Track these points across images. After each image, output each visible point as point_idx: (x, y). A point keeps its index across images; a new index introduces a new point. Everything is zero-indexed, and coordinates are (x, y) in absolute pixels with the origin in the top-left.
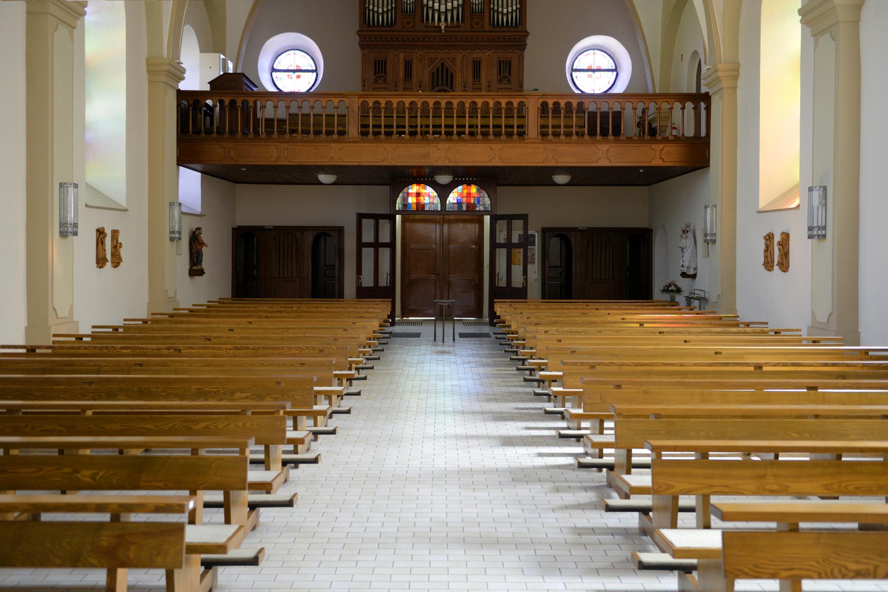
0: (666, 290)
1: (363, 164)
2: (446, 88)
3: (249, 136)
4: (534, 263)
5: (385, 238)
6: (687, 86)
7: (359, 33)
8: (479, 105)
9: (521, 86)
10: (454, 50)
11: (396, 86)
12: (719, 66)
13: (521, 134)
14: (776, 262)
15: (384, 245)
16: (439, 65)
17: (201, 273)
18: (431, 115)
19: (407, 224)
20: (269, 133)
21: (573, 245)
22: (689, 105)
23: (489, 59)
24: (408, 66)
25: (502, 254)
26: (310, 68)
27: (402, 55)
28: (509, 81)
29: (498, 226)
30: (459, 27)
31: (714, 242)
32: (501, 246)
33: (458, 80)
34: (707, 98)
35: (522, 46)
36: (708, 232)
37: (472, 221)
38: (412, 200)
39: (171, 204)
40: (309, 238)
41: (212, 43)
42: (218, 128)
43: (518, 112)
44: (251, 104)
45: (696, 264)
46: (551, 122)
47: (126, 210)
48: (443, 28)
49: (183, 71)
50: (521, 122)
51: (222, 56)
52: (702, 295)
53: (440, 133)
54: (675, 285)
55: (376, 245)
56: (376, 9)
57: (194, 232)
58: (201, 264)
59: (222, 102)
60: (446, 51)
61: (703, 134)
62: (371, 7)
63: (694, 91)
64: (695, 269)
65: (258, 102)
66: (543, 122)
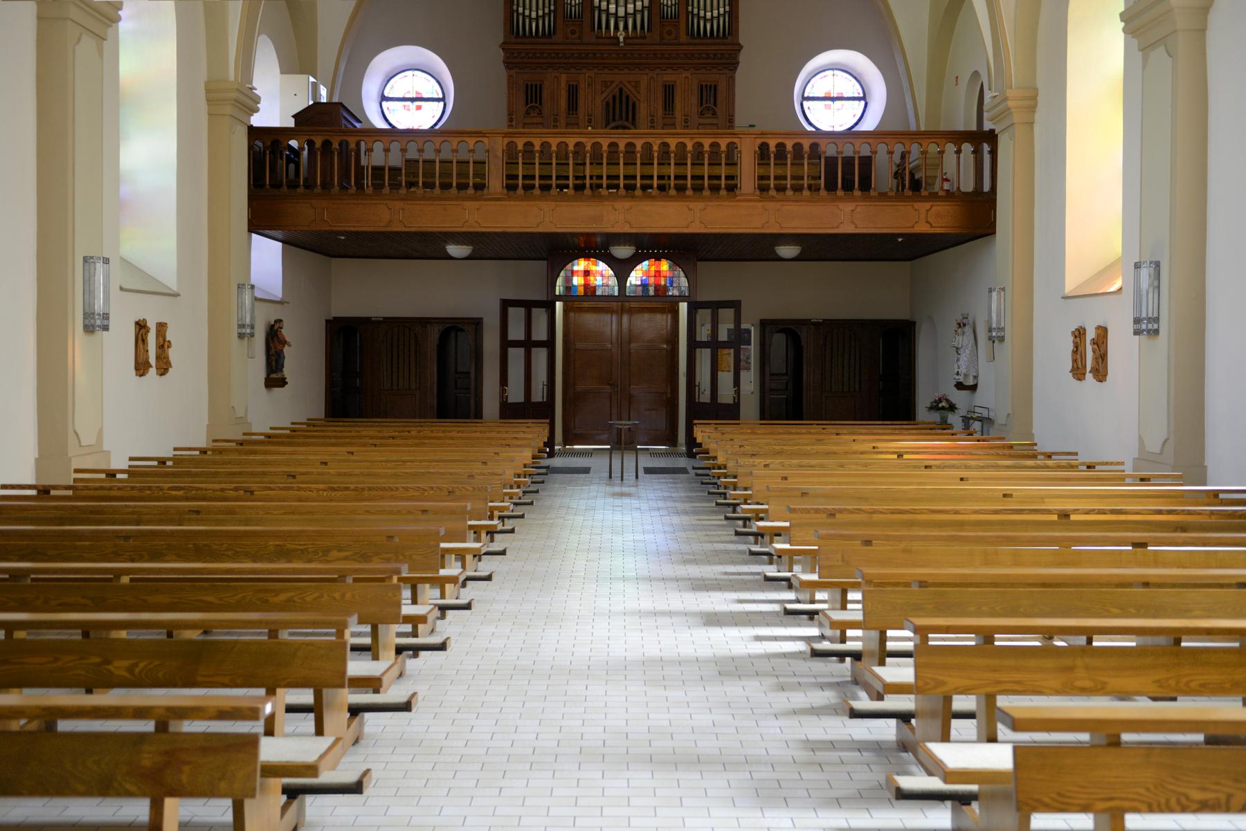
0: (935, 407)
1: (509, 230)
2: (626, 124)
3: (350, 191)
4: (749, 369)
5: (540, 334)
6: (964, 121)
7: (504, 46)
8: (673, 148)
9: (731, 120)
10: (637, 71)
11: (556, 120)
12: (1009, 93)
13: (731, 189)
14: (1088, 368)
15: (539, 344)
16: (617, 91)
17: (282, 383)
18: (605, 161)
19: (572, 315)
20: (378, 187)
21: (804, 343)
22: (967, 148)
23: (686, 82)
24: (573, 92)
25: (704, 356)
26: (435, 96)
27: (564, 77)
28: (714, 114)
29: (698, 317)
30: (645, 38)
31: (1002, 339)
32: (703, 345)
33: (643, 112)
34: (992, 137)
35: (733, 65)
36: (994, 326)
38: (577, 281)
39: (240, 287)
40: (434, 334)
41: (297, 60)
42: (306, 180)
43: (727, 158)
44: (352, 146)
45: (977, 371)
46: (773, 171)
47: (176, 295)
48: (621, 39)
49: (257, 100)
50: (731, 171)
51: (312, 79)
52: (985, 414)
53: (617, 187)
54: (947, 400)
55: (528, 344)
56: (527, 12)
57: (272, 326)
58: (281, 370)
59: (311, 143)
60: (626, 71)
61: (987, 188)
62: (521, 10)
63: (974, 128)
64: (975, 377)
65: (363, 144)
66: (762, 171)
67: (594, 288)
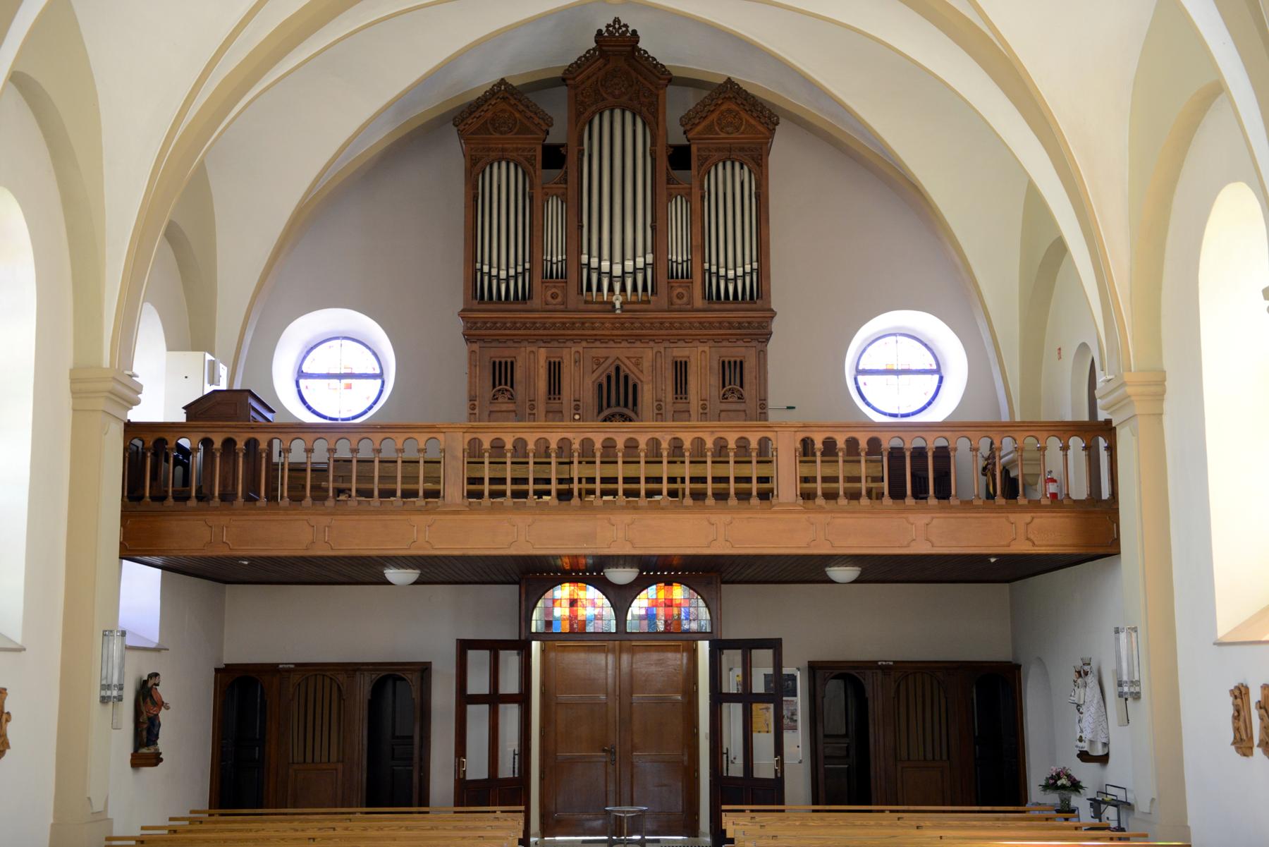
0: (1051, 785)
1: (471, 553)
2: (625, 411)
3: (258, 504)
4: (794, 729)
5: (510, 685)
6: (1072, 409)
7: (464, 314)
8: (687, 445)
9: (763, 405)
10: (638, 344)
11: (532, 407)
12: (1127, 377)
13: (765, 496)
14: (1256, 741)
15: (509, 699)
17: (155, 760)
18: (598, 461)
19: (552, 655)
20: (296, 496)
21: (869, 694)
22: (1076, 443)
23: (703, 361)
24: (555, 371)
25: (733, 714)
26: (370, 371)
27: (543, 353)
28: (741, 397)
29: (724, 658)
30: (648, 302)
31: (1137, 696)
32: (732, 698)
33: (647, 396)
34: (1108, 429)
35: (764, 336)
36: (1125, 678)
37: (676, 649)
38: (561, 612)
39: (106, 634)
40: (363, 688)
41: (191, 333)
42: (199, 490)
43: (759, 454)
44: (263, 446)
45: (1108, 737)
46: (819, 470)
47: (21, 650)
48: (618, 306)
49: (138, 389)
50: (764, 471)
51: (209, 357)
52: (1121, 796)
53: (614, 493)
54: (1069, 777)
55: (494, 699)
56: (494, 272)
57: (145, 682)
58: (155, 743)
59: (207, 442)
60: (624, 344)
61: (1106, 494)
62: (486, 269)
63: (1086, 418)
64: (1105, 745)
65: (276, 443)
66: (806, 471)
67: (584, 623)
